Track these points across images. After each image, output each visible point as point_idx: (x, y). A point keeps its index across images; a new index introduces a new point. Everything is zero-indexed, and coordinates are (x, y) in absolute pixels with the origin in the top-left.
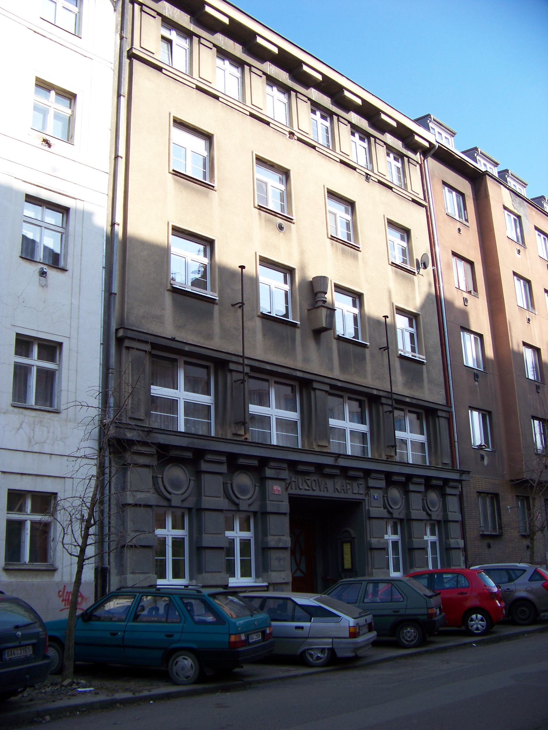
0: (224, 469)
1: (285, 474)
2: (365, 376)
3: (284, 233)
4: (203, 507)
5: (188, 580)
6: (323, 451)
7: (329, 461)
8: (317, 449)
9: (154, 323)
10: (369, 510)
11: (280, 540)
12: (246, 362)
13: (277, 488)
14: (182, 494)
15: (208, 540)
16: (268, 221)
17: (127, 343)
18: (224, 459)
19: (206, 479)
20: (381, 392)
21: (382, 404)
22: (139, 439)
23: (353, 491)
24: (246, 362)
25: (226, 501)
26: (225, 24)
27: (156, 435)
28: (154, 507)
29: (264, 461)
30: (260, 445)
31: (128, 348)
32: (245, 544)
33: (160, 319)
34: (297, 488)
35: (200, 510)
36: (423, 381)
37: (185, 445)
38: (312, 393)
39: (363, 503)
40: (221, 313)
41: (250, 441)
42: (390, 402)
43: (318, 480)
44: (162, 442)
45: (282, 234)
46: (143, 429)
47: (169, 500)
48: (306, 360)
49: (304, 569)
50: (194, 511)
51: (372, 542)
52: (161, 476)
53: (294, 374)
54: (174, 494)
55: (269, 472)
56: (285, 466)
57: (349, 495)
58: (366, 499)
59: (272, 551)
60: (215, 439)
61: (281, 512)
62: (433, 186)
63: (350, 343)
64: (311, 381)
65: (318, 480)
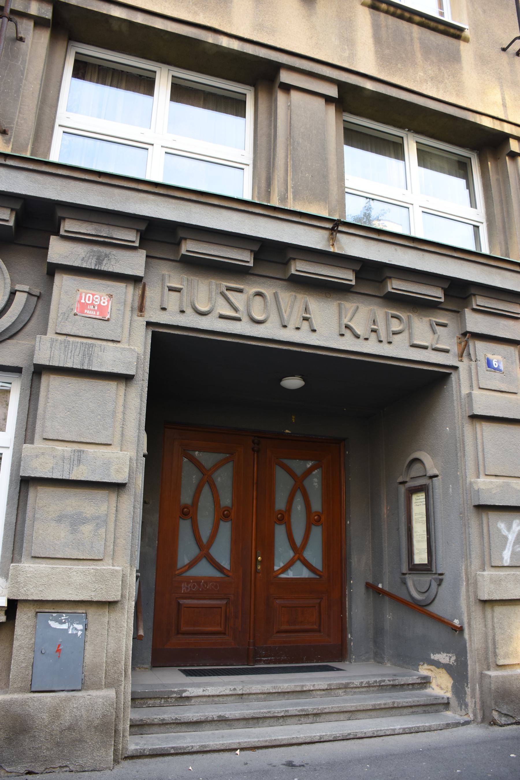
1: (134, 263)
10: (469, 395)
20: (505, 125)
21: (287, 88)
34: (189, 311)
39: (454, 377)
55: (59, 251)
57: (399, 350)
58: (463, 366)
61: (95, 368)
64: (278, 67)
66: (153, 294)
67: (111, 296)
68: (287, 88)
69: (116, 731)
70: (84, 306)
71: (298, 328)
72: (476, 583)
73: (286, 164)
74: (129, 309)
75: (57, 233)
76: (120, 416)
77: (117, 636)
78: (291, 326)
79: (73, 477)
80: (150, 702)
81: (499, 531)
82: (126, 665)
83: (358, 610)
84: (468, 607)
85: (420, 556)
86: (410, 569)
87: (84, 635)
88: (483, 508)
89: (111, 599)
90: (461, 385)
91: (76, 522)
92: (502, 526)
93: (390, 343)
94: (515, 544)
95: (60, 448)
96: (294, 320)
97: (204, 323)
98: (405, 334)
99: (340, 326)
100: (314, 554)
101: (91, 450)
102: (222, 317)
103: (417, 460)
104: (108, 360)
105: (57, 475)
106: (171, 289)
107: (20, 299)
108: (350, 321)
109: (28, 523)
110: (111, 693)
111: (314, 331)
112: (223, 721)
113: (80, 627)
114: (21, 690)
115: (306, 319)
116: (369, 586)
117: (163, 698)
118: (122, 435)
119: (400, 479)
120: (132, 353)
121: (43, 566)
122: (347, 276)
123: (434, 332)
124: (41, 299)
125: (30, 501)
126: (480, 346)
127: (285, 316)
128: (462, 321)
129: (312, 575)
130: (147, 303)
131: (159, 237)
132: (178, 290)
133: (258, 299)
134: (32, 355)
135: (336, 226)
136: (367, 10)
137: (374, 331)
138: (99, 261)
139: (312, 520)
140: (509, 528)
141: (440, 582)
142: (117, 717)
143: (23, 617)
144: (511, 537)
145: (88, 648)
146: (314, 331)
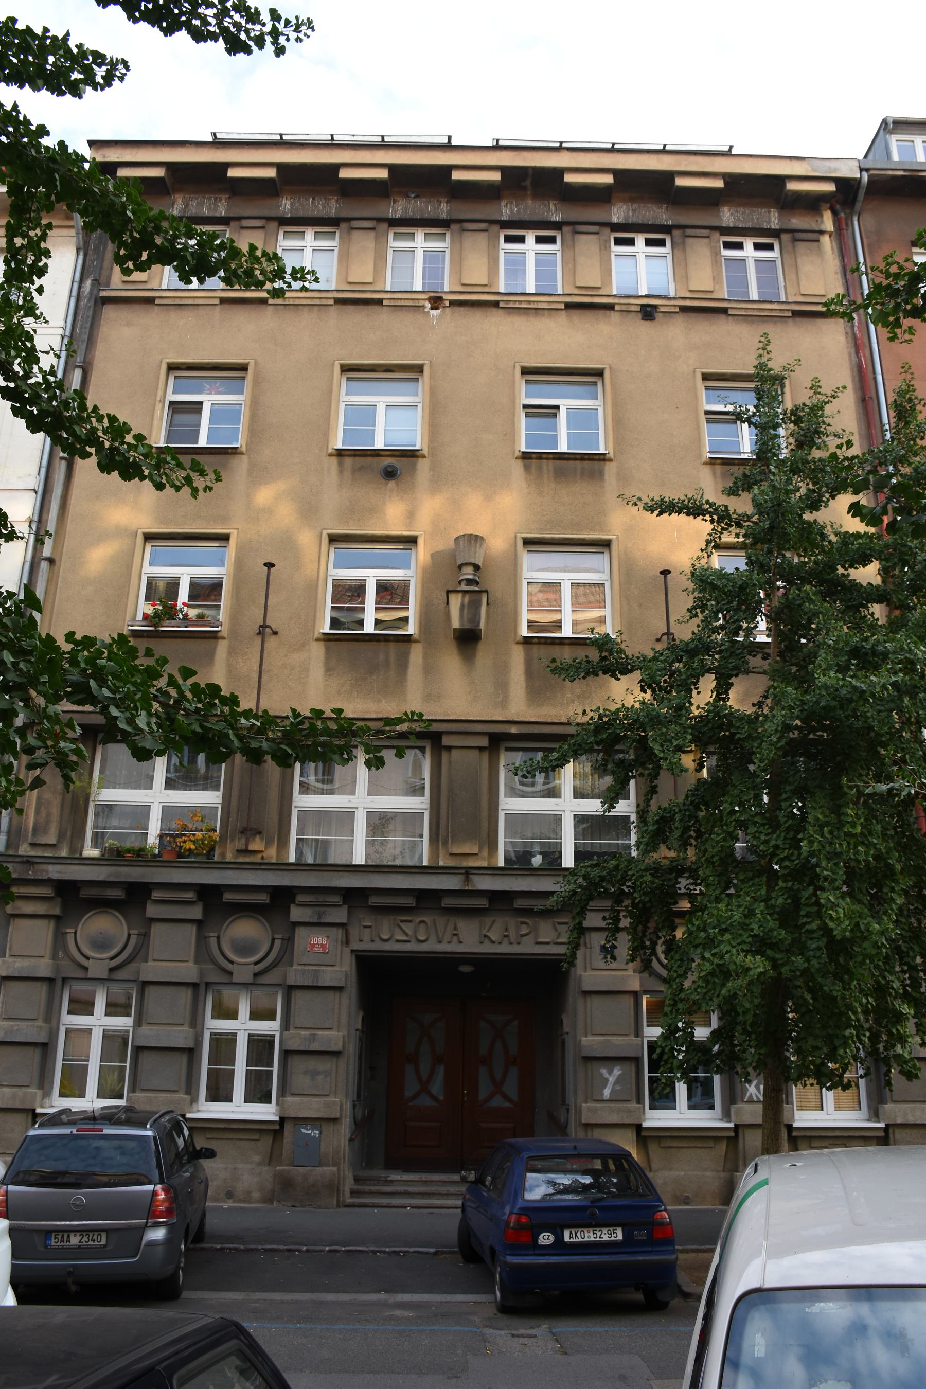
0: (196, 912)
1: (340, 915)
3: (397, 484)
11: (313, 1038)
18: (190, 895)
23: (544, 940)
26: (832, 193)
27: (45, 867)
29: (282, 897)
30: (263, 867)
34: (377, 939)
37: (101, 878)
40: (232, 651)
45: (392, 484)
46: (18, 860)
49: (514, 1095)
51: (583, 1043)
54: (94, 958)
63: (378, 641)
66: (354, 932)
67: (328, 937)
68: (449, 748)
69: (338, 1191)
70: (313, 946)
71: (449, 942)
72: (581, 1110)
73: (448, 813)
74: (339, 943)
75: (294, 902)
76: (337, 1011)
77: (340, 1138)
78: (445, 940)
79: (311, 1049)
80: (368, 1182)
81: (601, 1075)
82: (344, 1154)
84: (575, 1128)
87: (320, 1136)
88: (589, 1059)
89: (333, 1117)
91: (314, 1074)
92: (604, 1071)
93: (519, 943)
94: (615, 1084)
95: (303, 1032)
96: (447, 937)
97: (387, 947)
98: (532, 935)
101: (320, 1032)
102: (398, 941)
104: (329, 977)
105: (302, 1048)
107: (278, 943)
108: (488, 931)
109: (289, 1075)
110: (335, 1169)
111: (461, 942)
113: (317, 1132)
114: (288, 1165)
117: (377, 1180)
118: (339, 1022)
120: (341, 970)
121: (297, 1099)
123: (556, 930)
124: (289, 941)
125: (289, 1063)
127: (440, 935)
130: (351, 938)
131: (354, 898)
132: (370, 927)
133: (422, 925)
134: (285, 978)
136: (521, 647)
137: (505, 936)
138: (320, 917)
140: (610, 1073)
142: (339, 1183)
143: (288, 1127)
144: (612, 1079)
145: (323, 1144)
146: (461, 942)
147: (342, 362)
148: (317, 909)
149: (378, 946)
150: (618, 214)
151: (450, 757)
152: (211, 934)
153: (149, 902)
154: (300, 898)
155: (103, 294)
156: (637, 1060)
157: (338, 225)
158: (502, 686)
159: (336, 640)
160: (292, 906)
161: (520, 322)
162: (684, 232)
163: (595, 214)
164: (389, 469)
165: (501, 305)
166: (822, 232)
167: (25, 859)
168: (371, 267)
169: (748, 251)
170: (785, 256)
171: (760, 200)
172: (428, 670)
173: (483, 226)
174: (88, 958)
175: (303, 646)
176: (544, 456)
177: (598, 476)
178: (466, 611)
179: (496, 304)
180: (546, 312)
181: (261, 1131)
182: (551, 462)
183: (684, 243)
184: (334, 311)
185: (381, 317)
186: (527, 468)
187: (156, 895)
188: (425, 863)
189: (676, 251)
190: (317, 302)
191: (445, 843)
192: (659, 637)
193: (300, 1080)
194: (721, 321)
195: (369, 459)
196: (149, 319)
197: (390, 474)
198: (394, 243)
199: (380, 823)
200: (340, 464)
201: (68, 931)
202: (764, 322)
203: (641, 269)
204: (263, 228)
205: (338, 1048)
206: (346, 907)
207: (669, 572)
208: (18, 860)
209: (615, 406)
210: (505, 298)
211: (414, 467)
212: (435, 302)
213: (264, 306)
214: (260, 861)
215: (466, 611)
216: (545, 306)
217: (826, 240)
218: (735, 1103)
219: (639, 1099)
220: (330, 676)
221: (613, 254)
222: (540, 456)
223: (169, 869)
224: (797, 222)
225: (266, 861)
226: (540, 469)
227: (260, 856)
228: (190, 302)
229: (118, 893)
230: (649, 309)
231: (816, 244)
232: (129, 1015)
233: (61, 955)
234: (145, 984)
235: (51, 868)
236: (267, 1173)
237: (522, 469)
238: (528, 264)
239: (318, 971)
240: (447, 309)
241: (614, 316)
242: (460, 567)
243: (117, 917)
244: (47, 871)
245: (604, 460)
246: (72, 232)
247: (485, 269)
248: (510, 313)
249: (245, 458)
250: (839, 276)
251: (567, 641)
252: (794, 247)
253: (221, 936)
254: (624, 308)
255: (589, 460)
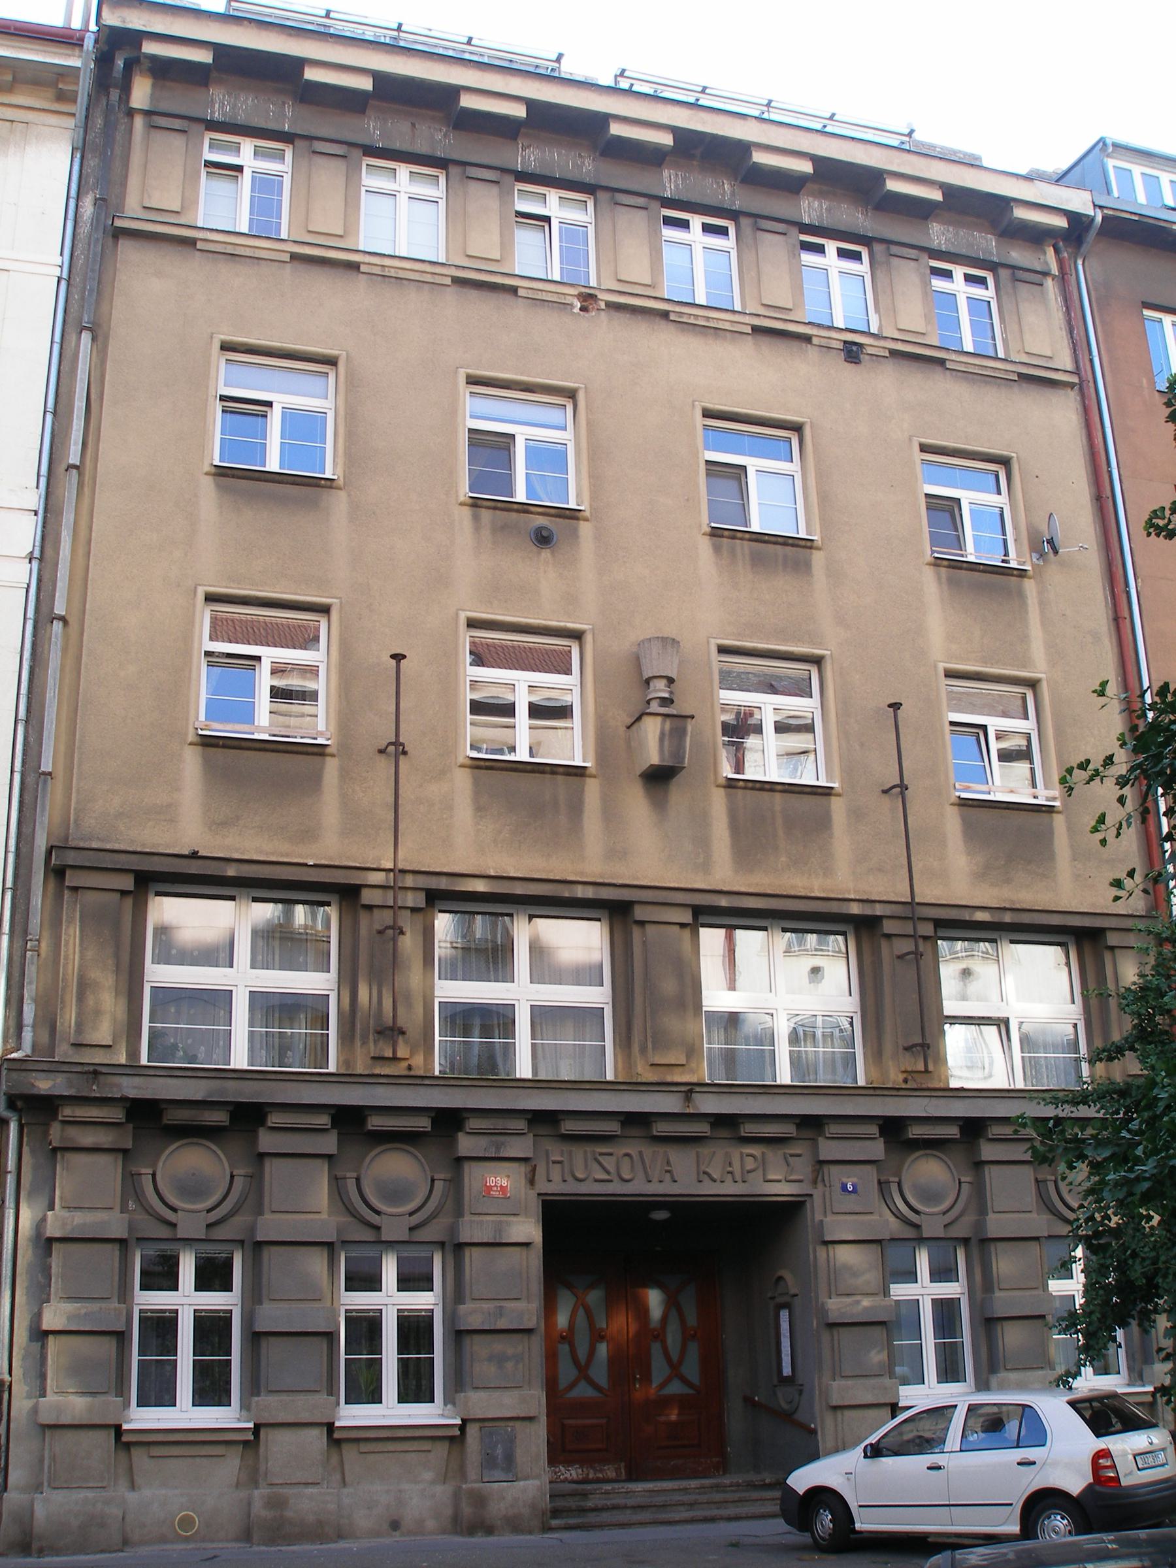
1: (519, 1147)
2: (828, 871)
3: (553, 553)
4: (990, 1235)
5: (973, 1384)
6: (669, 1079)
7: (668, 1103)
8: (650, 1076)
9: (150, 824)
10: (822, 1221)
12: (409, 881)
13: (501, 1179)
14: (944, 1213)
15: (1003, 1302)
16: (501, 529)
17: (71, 879)
19: (993, 1175)
22: (72, 1092)
24: (409, 881)
25: (1046, 1217)
27: (117, 1079)
28: (1043, 1240)
31: (75, 889)
32: (945, 1311)
33: (167, 813)
35: (985, 1242)
36: (1051, 856)
37: (199, 1097)
38: (1108, 957)
39: (808, 1205)
40: (345, 775)
41: (421, 1073)
42: (908, 929)
43: (640, 1153)
44: (132, 1094)
45: (546, 554)
46: (79, 1069)
47: (917, 1227)
48: (616, 853)
50: (974, 1242)
52: (897, 1179)
53: (567, 895)
56: (521, 1124)
58: (817, 1194)
59: (477, 1338)
60: (872, 1091)
62: (1103, 323)
63: (543, 772)
65: (640, 1153)
78: (655, 1180)
79: (498, 1327)
83: (736, 1422)
85: (787, 1371)
86: (780, 1382)
90: (816, 1212)
95: (486, 1306)
97: (584, 1188)
99: (698, 1174)
100: (692, 1369)
102: (596, 1181)
103: (780, 1278)
105: (486, 1327)
106: (554, 1162)
110: (537, 1482)
112: (615, 1507)
115: (667, 1171)
116: (748, 1401)
119: (769, 1295)
121: (482, 1394)
122: (703, 1128)
126: (834, 1169)
128: (815, 1148)
129: (692, 1392)
133: (627, 1158)
135: (690, 1090)
136: (722, 790)
137: (667, 1171)
139: (687, 1336)
141: (801, 1392)
143: (472, 1431)
147: (470, 371)
148: (494, 1138)
149: (708, 1189)
150: (810, 209)
151: (644, 934)
152: (348, 1175)
153: (982, 1142)
154: (473, 1123)
155: (118, 223)
156: (330, 1336)
157: (292, 143)
158: (703, 842)
159: (487, 768)
160: (820, 1139)
161: (695, 344)
162: (888, 249)
163: (777, 205)
164: (545, 533)
165: (672, 317)
166: (1046, 274)
167: (91, 1068)
168: (496, 238)
169: (958, 285)
170: (1005, 298)
171: (980, 222)
172: (611, 814)
173: (641, 201)
174: (175, 1210)
175: (442, 774)
176: (739, 535)
177: (802, 568)
178: (666, 743)
179: (665, 315)
180: (728, 334)
181: (433, 1438)
182: (745, 543)
183: (888, 263)
184: (452, 296)
185: (517, 312)
186: (717, 549)
187: (274, 1119)
188: (610, 1077)
189: (878, 273)
190: (429, 278)
191: (643, 1050)
192: (383, 747)
193: (483, 1369)
194: (938, 374)
195: (514, 515)
196: (186, 271)
197: (543, 539)
198: (370, 180)
199: (273, 1008)
200: (476, 518)
201: (143, 1171)
202: (986, 383)
203: (838, 288)
204: (497, 182)
205: (530, 1326)
206: (131, 1126)
207: (404, 657)
208: (79, 1069)
209: (821, 476)
210: (678, 309)
211: (574, 534)
212: (585, 301)
213: (355, 274)
214: (406, 1073)
215: (666, 743)
216: (727, 326)
217: (1049, 283)
218: (258, 1395)
219: (332, 1390)
220: (481, 817)
221: (363, 189)
222: (734, 534)
223: (295, 1084)
224: (1018, 255)
225: (412, 1073)
226: (733, 552)
227: (404, 1064)
228: (248, 252)
229: (220, 1117)
230: (854, 348)
231: (1039, 288)
232: (228, 1288)
233: (131, 1205)
234: (259, 1245)
235: (125, 1081)
236: (443, 1492)
237: (711, 551)
238: (697, 262)
239: (501, 1222)
240: (603, 313)
241: (812, 352)
242: (648, 682)
243: (214, 1152)
244: (119, 1086)
245: (811, 548)
246: (71, 122)
247: (646, 262)
248: (683, 331)
249: (342, 494)
250: (1064, 333)
251: (779, 787)
252: (1014, 288)
253: (362, 1176)
254: (824, 342)
255: (793, 545)
